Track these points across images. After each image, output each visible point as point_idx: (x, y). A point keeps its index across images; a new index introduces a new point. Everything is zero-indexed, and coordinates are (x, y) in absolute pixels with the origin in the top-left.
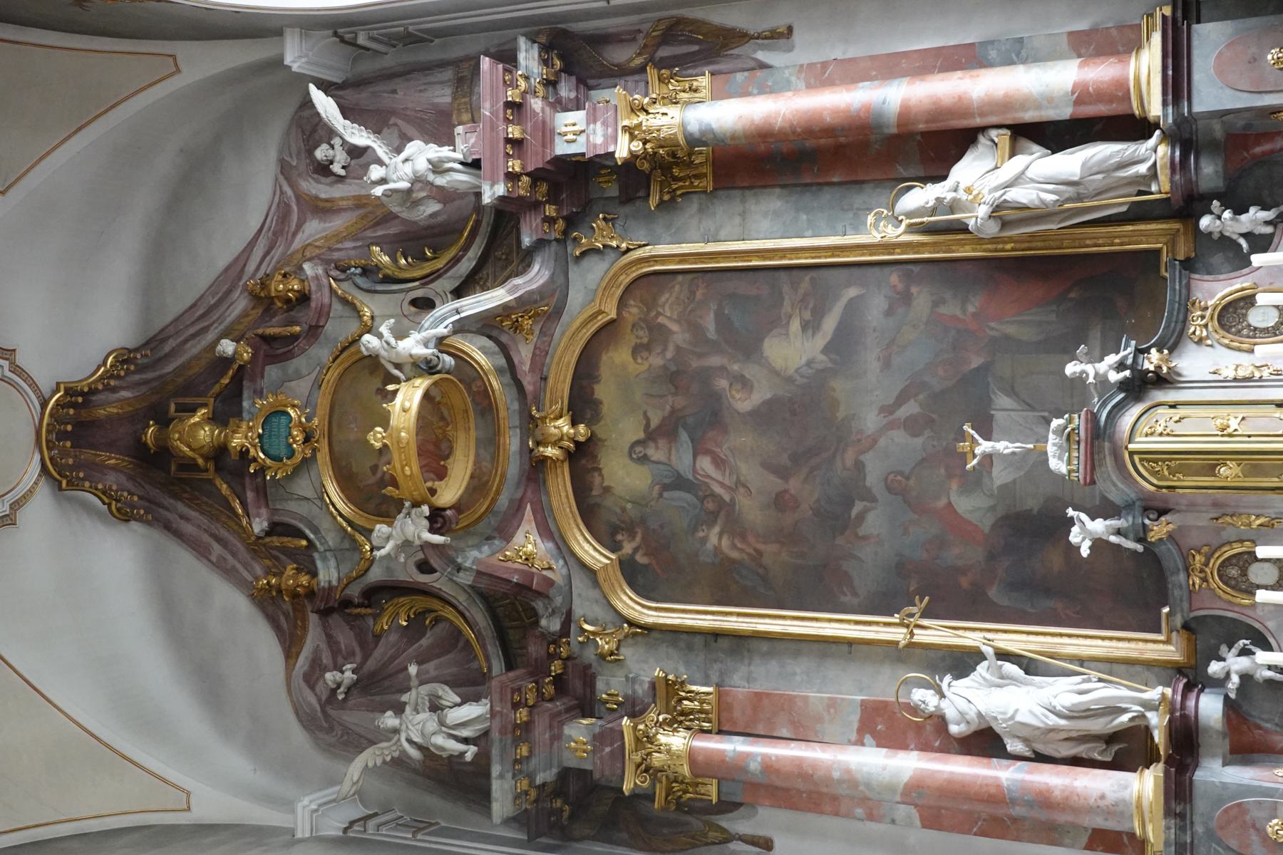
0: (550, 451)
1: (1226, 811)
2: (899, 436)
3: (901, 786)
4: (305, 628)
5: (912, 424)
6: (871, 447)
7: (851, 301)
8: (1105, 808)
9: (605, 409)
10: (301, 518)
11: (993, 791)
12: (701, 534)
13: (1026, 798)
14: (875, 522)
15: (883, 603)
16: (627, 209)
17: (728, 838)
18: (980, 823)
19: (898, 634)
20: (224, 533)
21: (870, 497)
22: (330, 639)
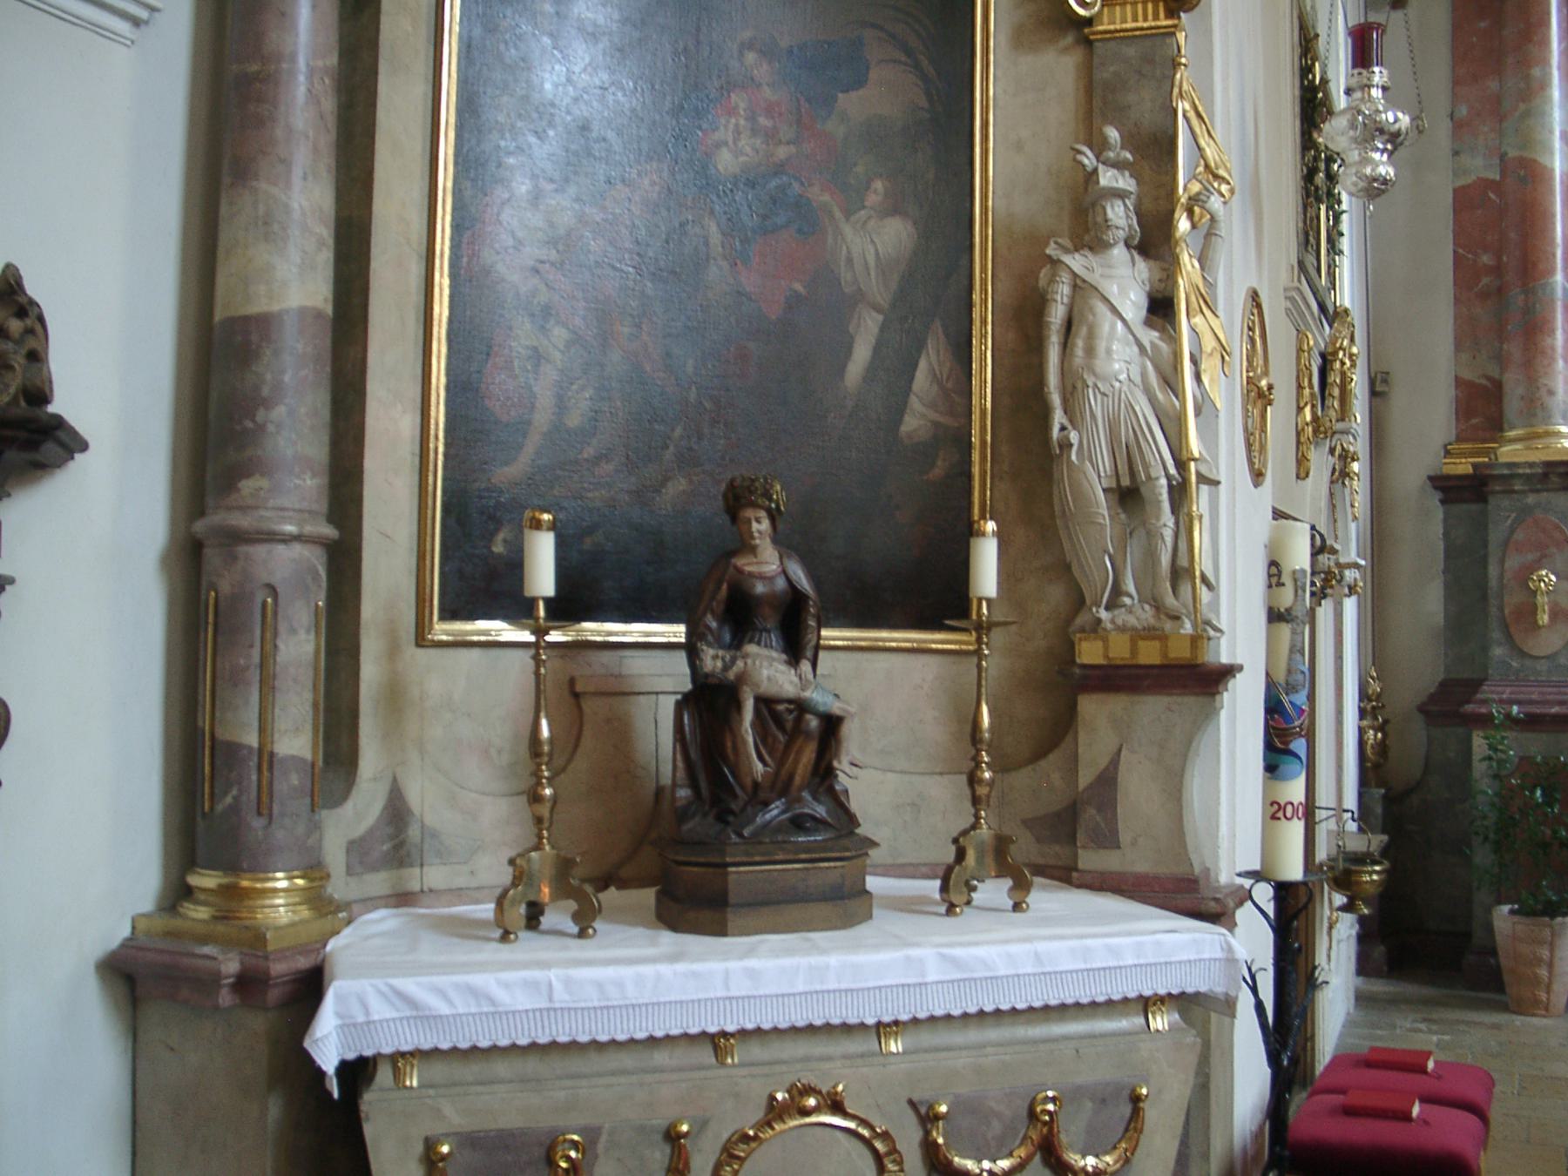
1: (1557, 527)
3: (1532, 156)
8: (1537, 395)
11: (1541, 267)
13: (1538, 306)
18: (1470, 256)
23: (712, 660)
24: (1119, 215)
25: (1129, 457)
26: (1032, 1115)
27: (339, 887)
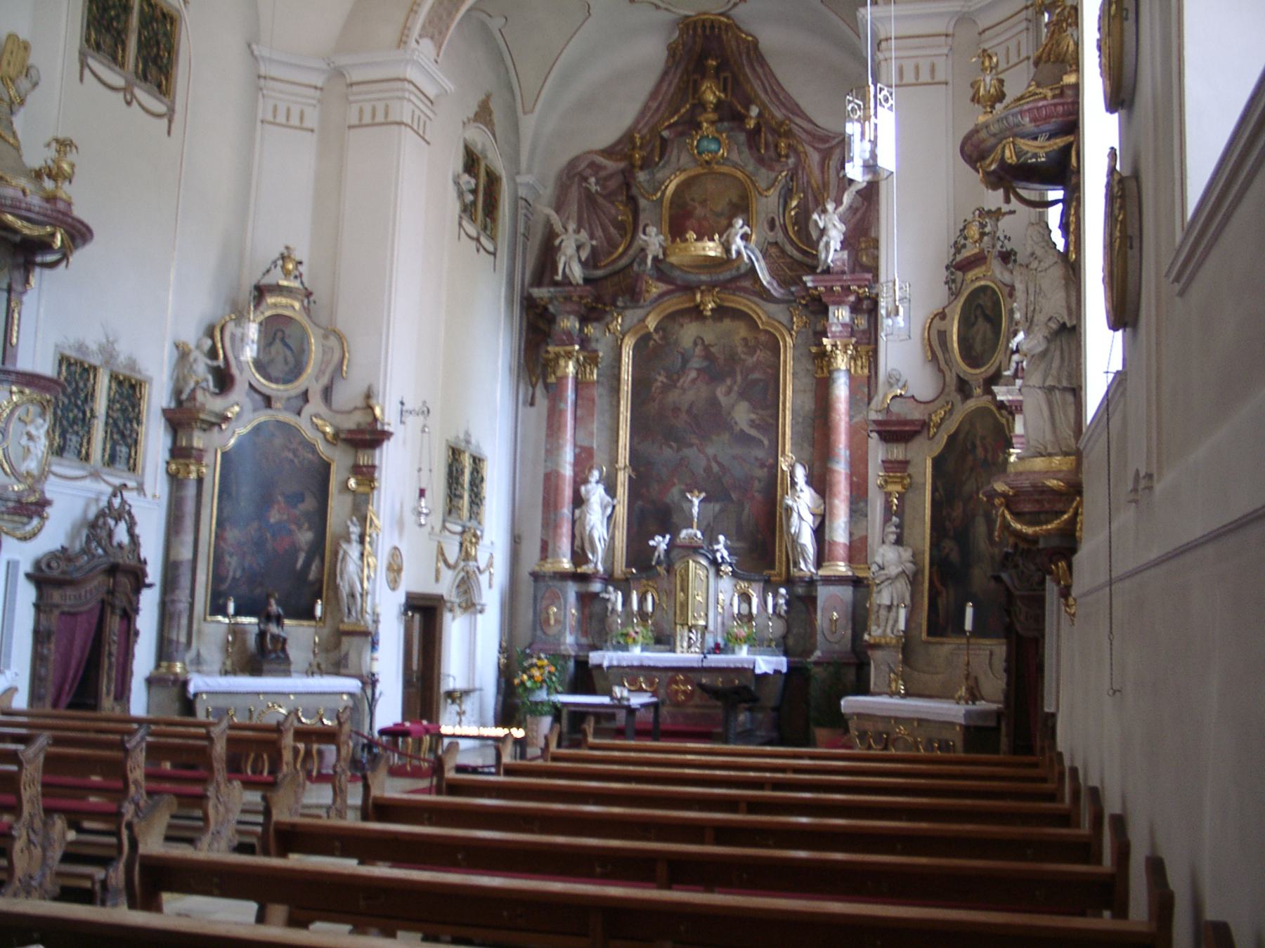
0: (698, 297)
2: (704, 463)
4: (616, 160)
5: (708, 469)
6: (699, 451)
7: (762, 442)
9: (719, 324)
10: (670, 157)
12: (662, 372)
14: (668, 453)
15: (636, 457)
16: (811, 333)
17: (534, 386)
19: (621, 463)
20: (663, 108)
21: (679, 449)
22: (611, 176)
23: (262, 626)
24: (354, 537)
25: (352, 587)
26: (318, 713)
27: (188, 668)
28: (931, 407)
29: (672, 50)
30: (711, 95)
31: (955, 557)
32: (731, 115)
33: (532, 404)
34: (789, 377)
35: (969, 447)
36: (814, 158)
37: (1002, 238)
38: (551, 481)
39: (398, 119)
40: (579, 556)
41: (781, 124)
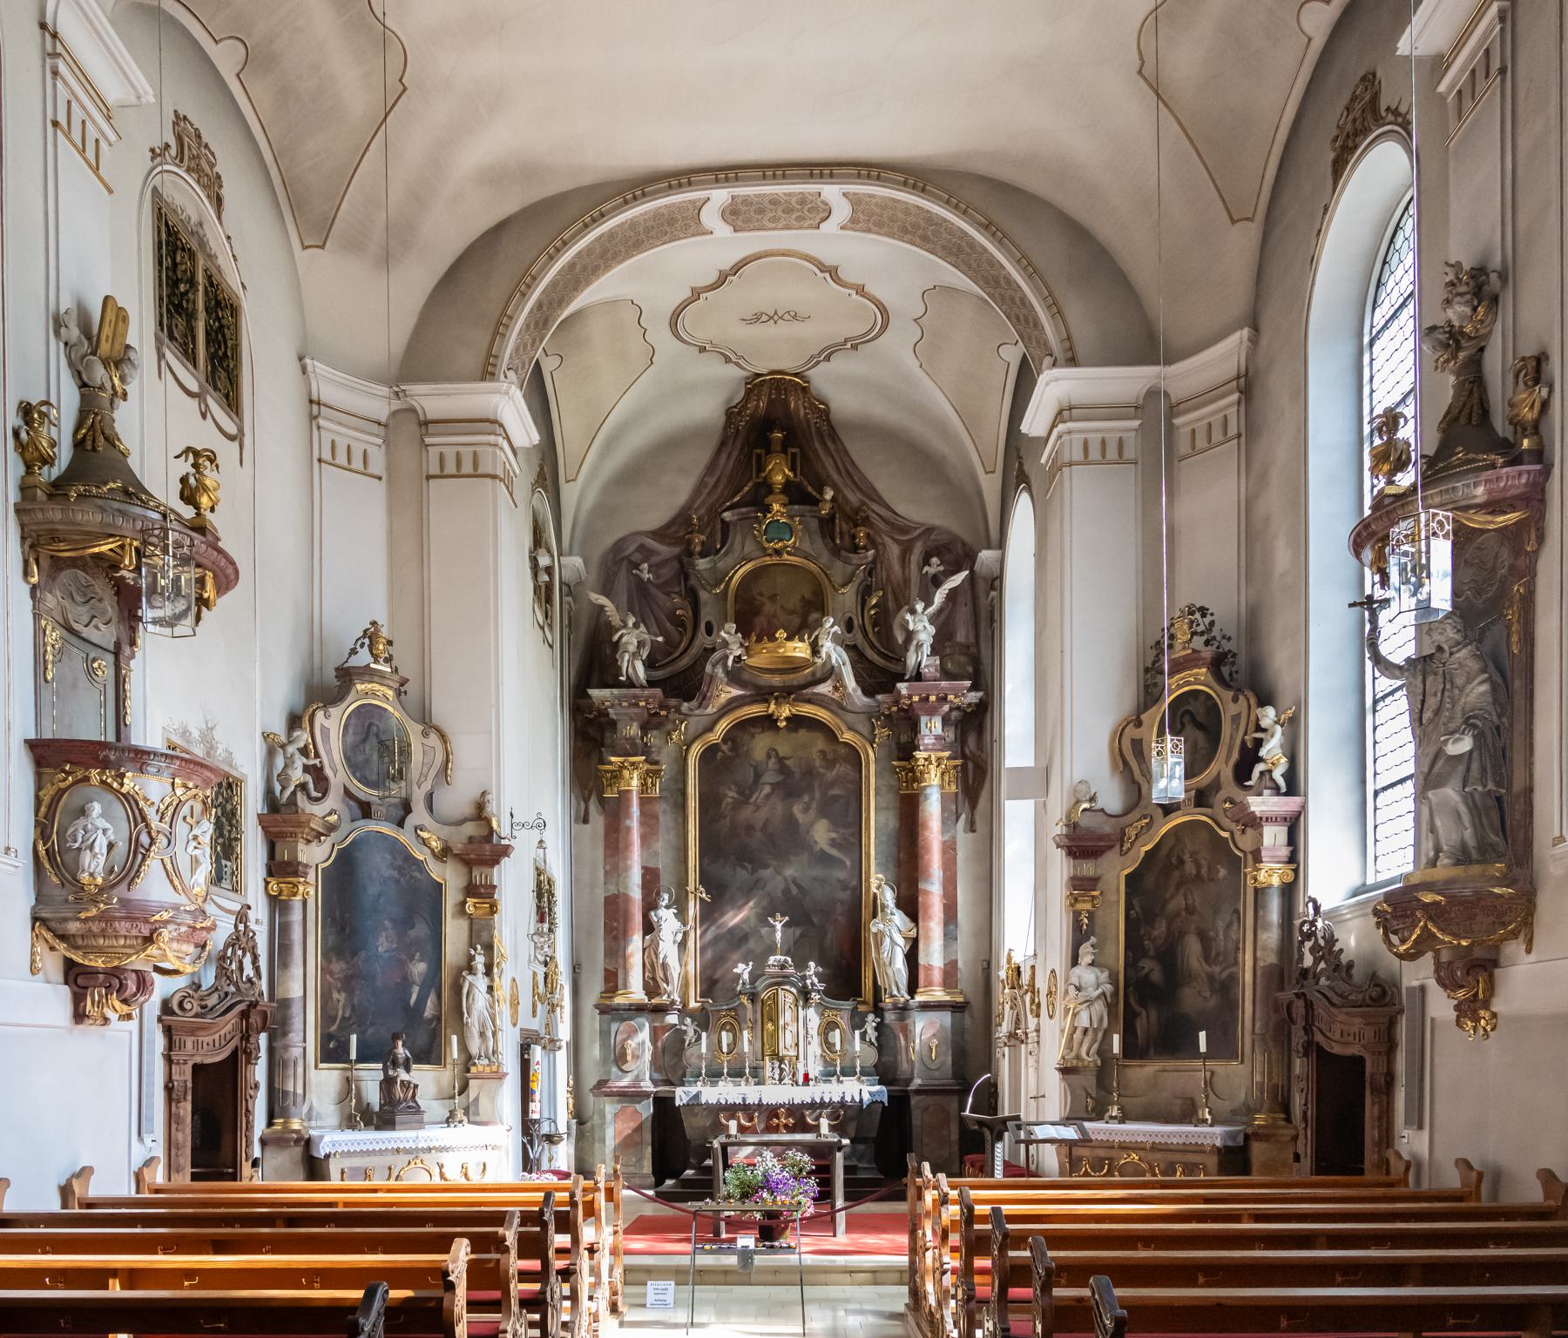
4: (669, 545)
5: (787, 891)
10: (732, 545)
17: (586, 801)
20: (721, 486)
21: (754, 871)
28: (1123, 821)
29: (731, 414)
30: (780, 473)
31: (1157, 976)
32: (796, 495)
33: (586, 821)
34: (872, 793)
35: (1174, 860)
36: (894, 551)
37: (1219, 639)
38: (615, 907)
39: (490, 471)
40: (652, 988)
41: (857, 511)
